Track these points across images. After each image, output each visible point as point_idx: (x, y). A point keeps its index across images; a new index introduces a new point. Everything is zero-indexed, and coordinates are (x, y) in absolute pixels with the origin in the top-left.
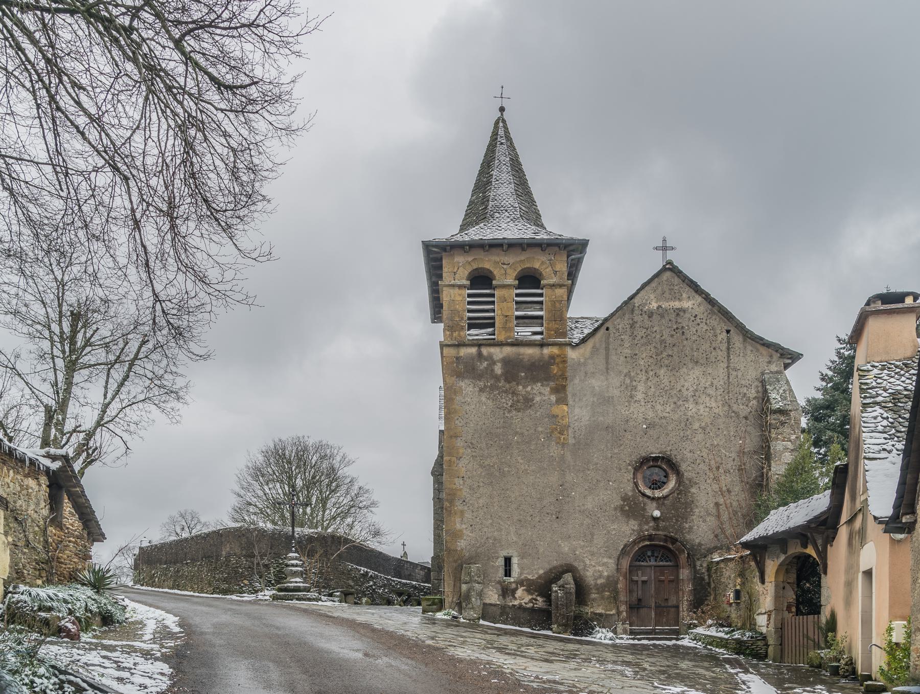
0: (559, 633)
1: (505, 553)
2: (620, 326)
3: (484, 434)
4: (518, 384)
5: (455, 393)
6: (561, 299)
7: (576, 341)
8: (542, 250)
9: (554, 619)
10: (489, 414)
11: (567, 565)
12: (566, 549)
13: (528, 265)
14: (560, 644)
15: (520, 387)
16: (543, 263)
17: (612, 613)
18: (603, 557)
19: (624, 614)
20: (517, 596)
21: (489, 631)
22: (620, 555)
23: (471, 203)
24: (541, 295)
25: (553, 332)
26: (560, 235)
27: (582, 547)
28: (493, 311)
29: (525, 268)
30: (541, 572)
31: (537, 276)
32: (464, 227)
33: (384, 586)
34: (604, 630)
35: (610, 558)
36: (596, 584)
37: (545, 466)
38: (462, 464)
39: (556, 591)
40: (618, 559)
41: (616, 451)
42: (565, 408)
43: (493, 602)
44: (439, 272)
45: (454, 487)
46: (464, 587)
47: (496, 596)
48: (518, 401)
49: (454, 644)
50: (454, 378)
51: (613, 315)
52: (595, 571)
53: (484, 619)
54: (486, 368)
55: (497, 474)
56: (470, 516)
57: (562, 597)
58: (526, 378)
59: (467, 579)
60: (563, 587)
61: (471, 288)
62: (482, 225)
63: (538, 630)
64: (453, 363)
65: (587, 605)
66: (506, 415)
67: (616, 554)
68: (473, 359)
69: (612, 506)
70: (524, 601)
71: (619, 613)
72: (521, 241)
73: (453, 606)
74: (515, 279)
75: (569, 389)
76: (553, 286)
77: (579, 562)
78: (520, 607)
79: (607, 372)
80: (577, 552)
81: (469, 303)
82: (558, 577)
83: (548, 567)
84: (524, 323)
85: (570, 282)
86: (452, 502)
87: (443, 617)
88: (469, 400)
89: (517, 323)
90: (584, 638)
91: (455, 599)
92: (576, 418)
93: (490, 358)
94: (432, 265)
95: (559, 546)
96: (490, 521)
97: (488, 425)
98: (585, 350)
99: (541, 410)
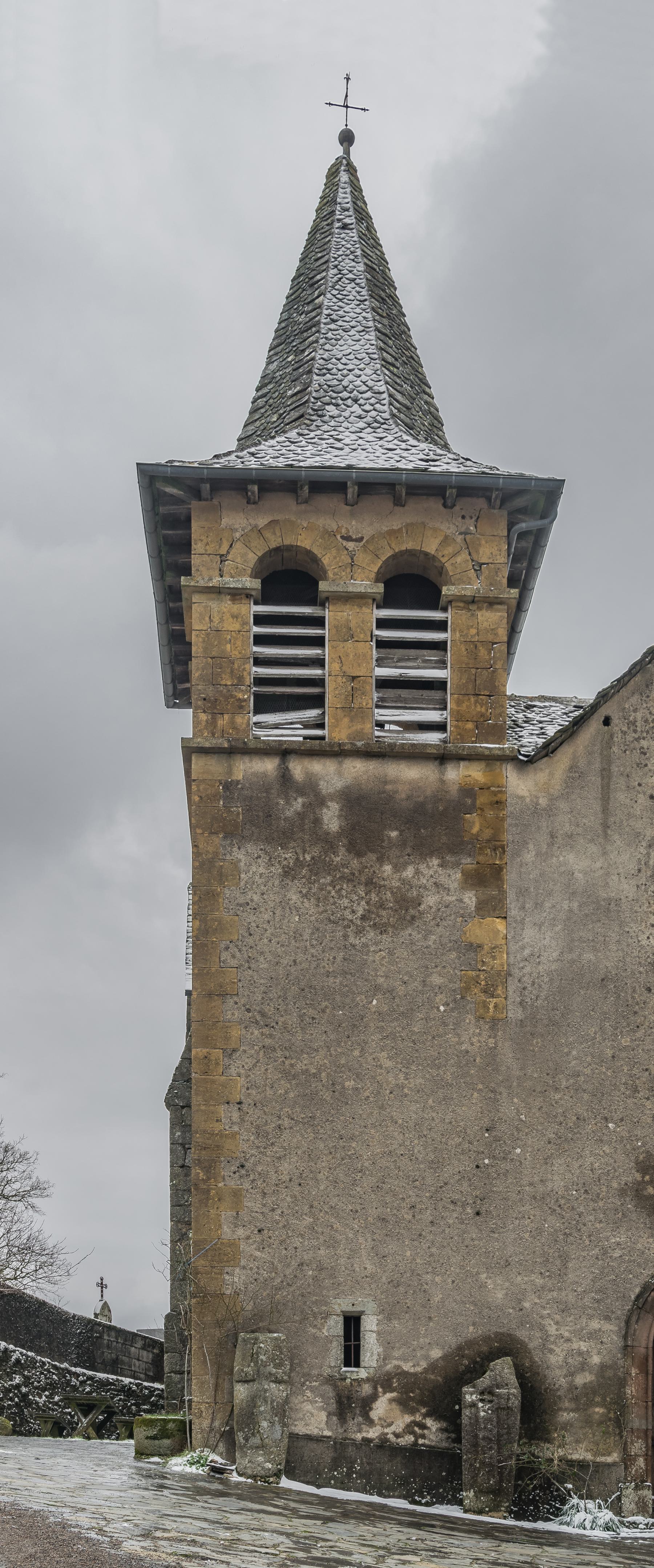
0: (480, 1512)
1: (343, 1304)
2: (639, 715)
3: (295, 989)
4: (381, 860)
5: (222, 877)
6: (490, 637)
7: (529, 750)
8: (445, 505)
9: (466, 1476)
10: (306, 936)
11: (499, 1336)
12: (500, 1295)
13: (409, 545)
14: (486, 1544)
15: (388, 868)
16: (446, 540)
17: (609, 1460)
18: (591, 1317)
19: (641, 1462)
20: (374, 1415)
21: (304, 1509)
22: (631, 1312)
23: (266, 379)
24: (441, 626)
25: (470, 726)
26: (491, 468)
27: (540, 1291)
28: (319, 662)
29: (402, 553)
30: (436, 1353)
31: (432, 576)
32: (244, 442)
33: (52, 1387)
34: (590, 1504)
35: (607, 1318)
36: (572, 1387)
37: (448, 1076)
38: (238, 1066)
39: (473, 1405)
40: (628, 1322)
41: (625, 1041)
42: (500, 925)
43: (316, 1432)
44: (181, 559)
45: (218, 1127)
46: (241, 1392)
47: (323, 1416)
48: (381, 905)
49: (202, 1552)
50: (218, 839)
51: (621, 683)
52: (570, 1353)
53: (291, 1476)
54: (301, 816)
55: (327, 1096)
56: (257, 1207)
57: (488, 1420)
58: (403, 844)
59: (250, 1370)
60: (491, 1393)
61: (265, 600)
62: (293, 434)
63: (427, 1504)
64: (215, 797)
65: (549, 1441)
66: (352, 940)
67: (622, 1308)
68: (267, 789)
69: (615, 1185)
70: (393, 1428)
71: (627, 1460)
72: (392, 477)
73: (212, 1441)
74: (377, 580)
75: (510, 877)
76: (471, 602)
77: (532, 1328)
78: (383, 1444)
79: (606, 835)
80: (527, 1305)
81: (260, 640)
82: (477, 1369)
83: (452, 1341)
84: (399, 699)
85: (514, 592)
86: (210, 1167)
87: (189, 1469)
88: (256, 898)
89: (381, 699)
90: (540, 1525)
91: (217, 1424)
92: (527, 952)
93: (310, 788)
94: (165, 537)
95: (483, 1286)
96: (309, 1220)
97: (305, 965)
98: (551, 774)
99: (440, 929)
